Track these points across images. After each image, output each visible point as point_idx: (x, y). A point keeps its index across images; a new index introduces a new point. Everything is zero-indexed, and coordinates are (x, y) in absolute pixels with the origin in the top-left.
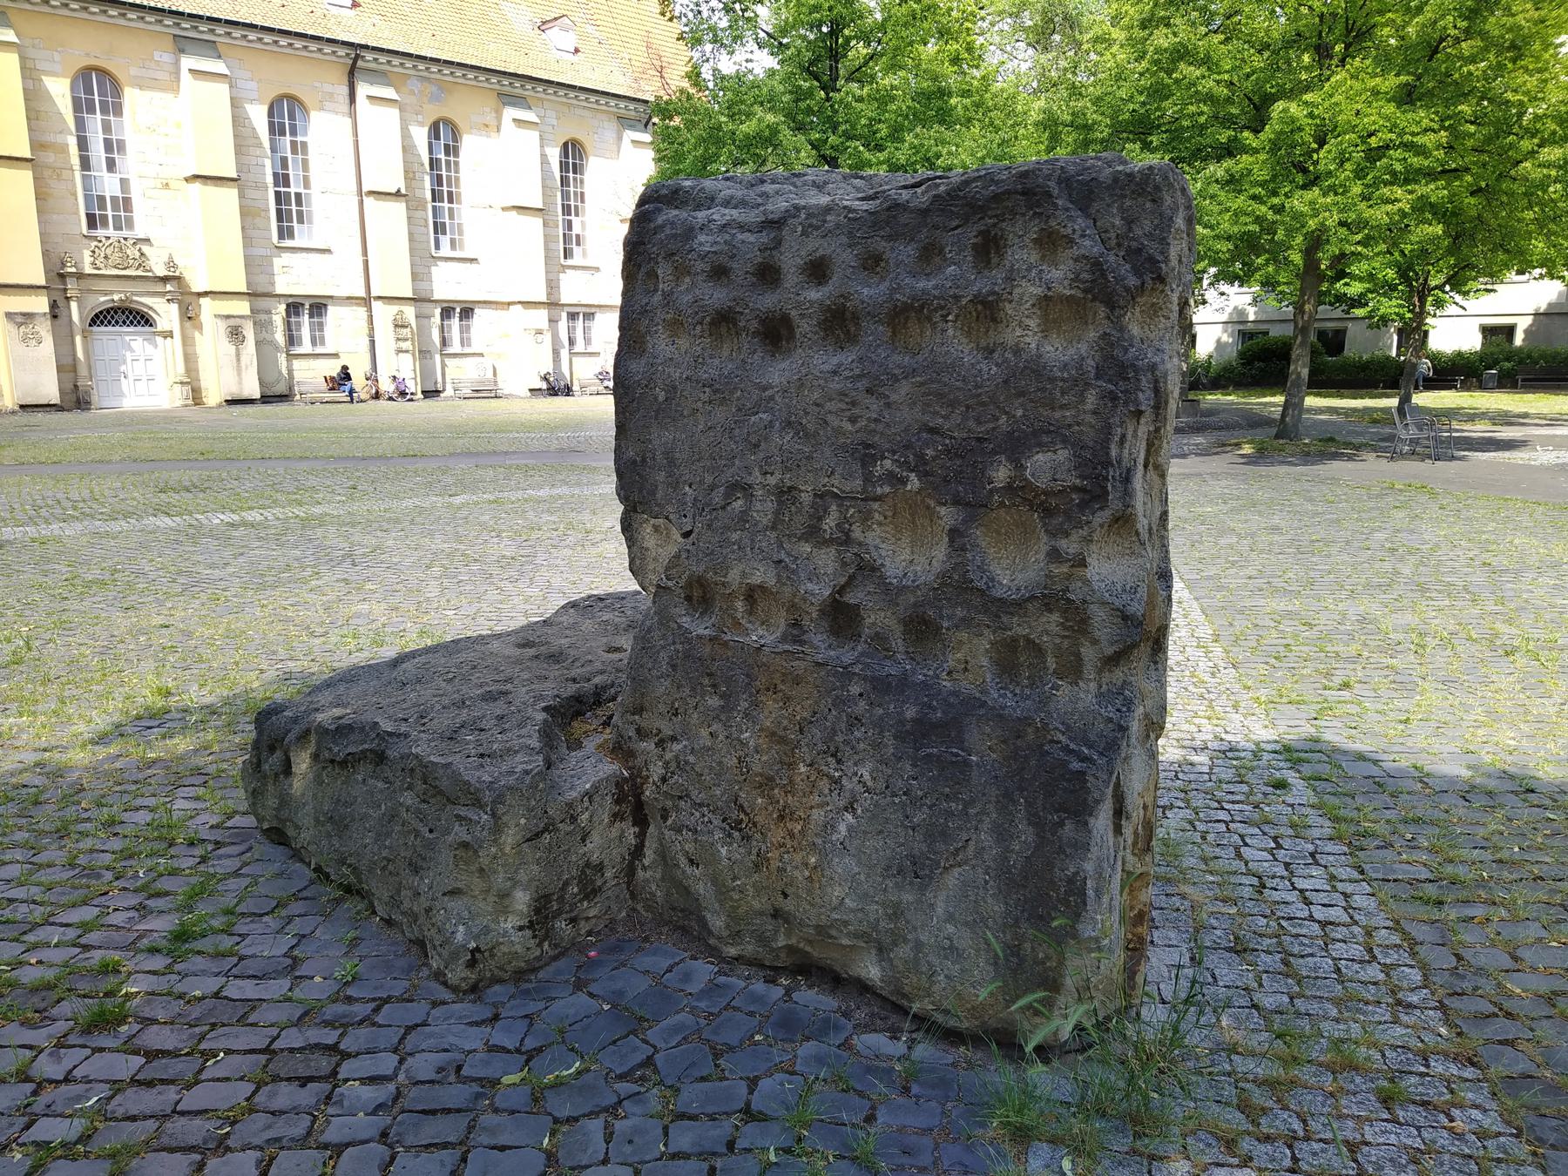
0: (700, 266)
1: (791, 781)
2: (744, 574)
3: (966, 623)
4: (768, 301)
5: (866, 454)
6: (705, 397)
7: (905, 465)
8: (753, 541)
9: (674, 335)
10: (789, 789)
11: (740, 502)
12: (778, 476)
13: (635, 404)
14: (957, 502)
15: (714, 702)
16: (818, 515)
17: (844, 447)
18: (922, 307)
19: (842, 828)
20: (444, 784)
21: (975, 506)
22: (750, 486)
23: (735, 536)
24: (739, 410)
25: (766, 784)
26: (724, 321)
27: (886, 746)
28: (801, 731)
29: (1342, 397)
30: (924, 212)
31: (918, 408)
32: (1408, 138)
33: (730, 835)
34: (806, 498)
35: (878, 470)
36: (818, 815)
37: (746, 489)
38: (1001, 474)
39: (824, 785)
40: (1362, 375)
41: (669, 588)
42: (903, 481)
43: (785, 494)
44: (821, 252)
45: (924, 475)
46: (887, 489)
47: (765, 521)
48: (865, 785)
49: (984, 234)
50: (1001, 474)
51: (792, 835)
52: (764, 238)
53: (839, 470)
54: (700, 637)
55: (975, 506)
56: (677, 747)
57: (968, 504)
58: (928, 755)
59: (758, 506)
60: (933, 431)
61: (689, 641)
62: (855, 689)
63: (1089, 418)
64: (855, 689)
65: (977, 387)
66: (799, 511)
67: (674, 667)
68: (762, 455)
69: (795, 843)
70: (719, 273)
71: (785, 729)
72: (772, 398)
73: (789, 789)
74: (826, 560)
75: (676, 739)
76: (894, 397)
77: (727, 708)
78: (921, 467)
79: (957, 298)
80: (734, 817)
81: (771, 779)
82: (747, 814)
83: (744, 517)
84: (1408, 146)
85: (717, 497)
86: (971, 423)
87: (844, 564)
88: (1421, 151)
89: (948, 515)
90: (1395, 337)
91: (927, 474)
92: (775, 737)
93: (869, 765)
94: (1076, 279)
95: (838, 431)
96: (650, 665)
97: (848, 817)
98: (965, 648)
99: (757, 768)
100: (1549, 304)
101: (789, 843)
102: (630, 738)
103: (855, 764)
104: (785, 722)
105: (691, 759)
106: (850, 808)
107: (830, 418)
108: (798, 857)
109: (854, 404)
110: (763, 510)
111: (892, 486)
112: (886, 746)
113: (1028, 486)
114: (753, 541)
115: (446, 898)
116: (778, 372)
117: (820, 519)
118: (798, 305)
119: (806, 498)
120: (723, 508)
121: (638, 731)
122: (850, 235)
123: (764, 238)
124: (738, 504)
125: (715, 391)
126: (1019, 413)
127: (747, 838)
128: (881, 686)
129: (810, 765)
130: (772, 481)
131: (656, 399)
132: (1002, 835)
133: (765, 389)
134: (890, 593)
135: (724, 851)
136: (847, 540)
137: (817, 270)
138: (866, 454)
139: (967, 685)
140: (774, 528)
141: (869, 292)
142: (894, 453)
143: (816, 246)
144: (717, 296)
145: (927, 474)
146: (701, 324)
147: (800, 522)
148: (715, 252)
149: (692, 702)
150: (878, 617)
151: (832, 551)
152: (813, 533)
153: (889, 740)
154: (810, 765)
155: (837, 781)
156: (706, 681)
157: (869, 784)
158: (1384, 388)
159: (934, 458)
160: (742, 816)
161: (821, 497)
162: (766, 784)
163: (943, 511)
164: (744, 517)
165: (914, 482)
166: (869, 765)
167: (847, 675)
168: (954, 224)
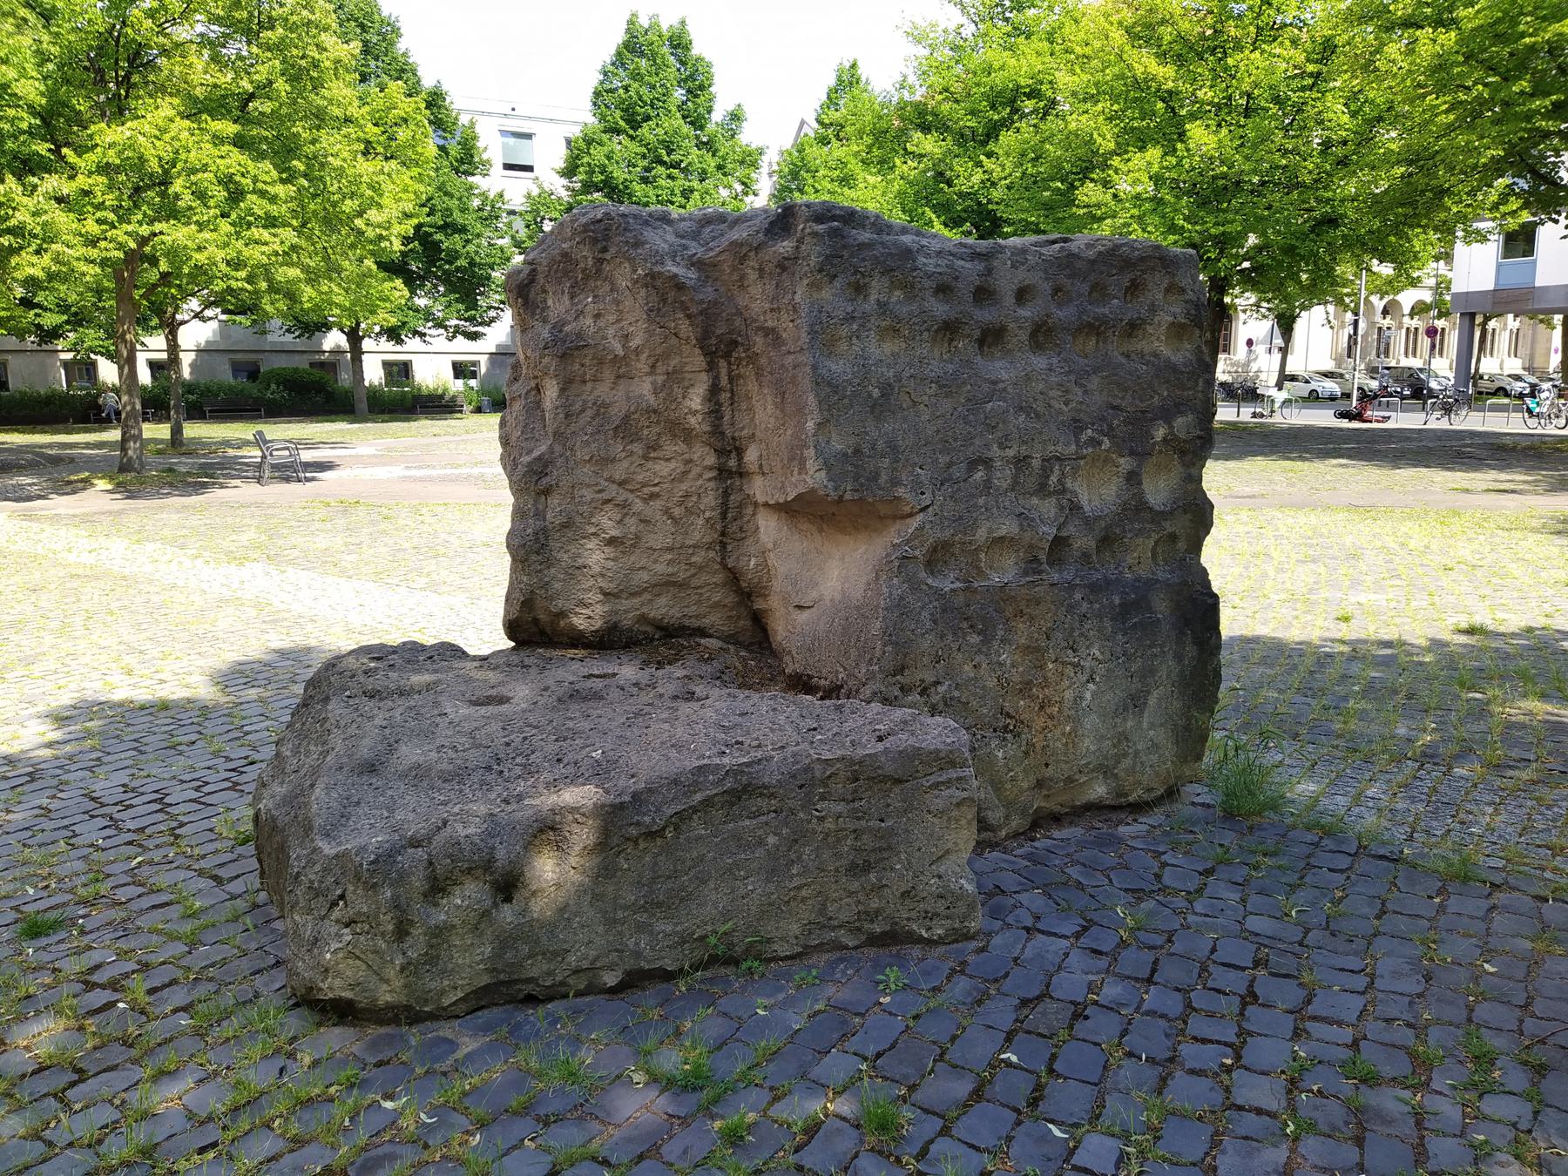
0: (927, 283)
1: (1045, 679)
2: (990, 530)
3: (1138, 534)
4: (985, 315)
5: (1077, 426)
6: (932, 392)
7: (1102, 433)
8: (997, 502)
9: (882, 339)
10: (1046, 683)
11: (980, 474)
12: (1015, 447)
13: (846, 401)
14: (1132, 453)
15: (974, 639)
16: (1045, 473)
17: (1063, 422)
18: (1100, 326)
19: (1088, 695)
20: (889, 769)
21: (1141, 454)
22: (991, 460)
23: (981, 501)
24: (969, 400)
25: (1025, 689)
26: (949, 329)
27: (1106, 628)
28: (1048, 638)
29: (69, 433)
30: (1093, 262)
31: (1105, 393)
32: (260, 185)
33: (1004, 739)
34: (1036, 463)
35: (1084, 437)
36: (1069, 695)
37: (987, 463)
38: (1160, 433)
39: (1069, 671)
40: (46, 410)
41: (915, 557)
42: (1100, 443)
43: (1021, 462)
44: (1027, 282)
45: (1112, 437)
46: (1090, 450)
47: (1005, 485)
48: (1097, 659)
49: (1133, 281)
50: (1160, 433)
51: (1051, 717)
52: (980, 266)
53: (1062, 440)
54: (953, 590)
55: (1141, 454)
56: (941, 689)
57: (1138, 454)
58: (1135, 624)
59: (999, 475)
60: (1115, 408)
61: (943, 596)
62: (1078, 596)
63: (1200, 395)
64: (1078, 596)
65: (1139, 378)
66: (1030, 474)
67: (935, 622)
68: (1000, 434)
69: (1055, 722)
70: (943, 290)
71: (1037, 640)
72: (1005, 389)
73: (1046, 683)
74: (1048, 507)
75: (939, 683)
76: (1090, 386)
77: (987, 641)
78: (1110, 433)
79: (1121, 320)
80: (1001, 724)
81: (1029, 683)
82: (1011, 717)
83: (988, 484)
84: (262, 194)
85: (958, 472)
86: (1137, 402)
87: (1062, 508)
88: (273, 199)
89: (1125, 463)
90: (63, 372)
91: (1114, 437)
92: (1028, 650)
93: (1096, 646)
94: (1188, 313)
95: (1060, 412)
96: (913, 627)
97: (1091, 686)
98: (1140, 548)
99: (1017, 679)
100: (207, 342)
101: (1050, 723)
102: (896, 697)
103: (1087, 648)
104: (1036, 635)
105: (956, 694)
106: (1091, 679)
107: (1053, 403)
108: (1058, 732)
109: (1067, 391)
110: (1003, 477)
111: (1094, 447)
112: (1106, 628)
113: (1176, 438)
114: (997, 502)
115: (934, 867)
116: (1000, 369)
117: (1048, 477)
118: (1016, 320)
119: (1036, 463)
120: (965, 480)
121: (902, 689)
122: (1046, 272)
123: (980, 266)
124: (979, 475)
125: (941, 387)
126: (1165, 394)
127: (1017, 735)
128: (1095, 588)
129: (1056, 661)
130: (1010, 453)
131: (870, 396)
132: (1179, 657)
133: (995, 383)
134: (1088, 522)
135: (1000, 754)
136: (1064, 491)
137: (1022, 295)
138: (1077, 426)
139: (1143, 572)
140: (1013, 490)
141: (1063, 314)
142: (1093, 424)
143: (1022, 276)
144: (940, 309)
145: (1114, 437)
146: (928, 330)
147: (1031, 482)
148: (940, 274)
149: (955, 646)
150: (1083, 541)
151: (1053, 500)
152: (1042, 490)
153: (1108, 624)
154: (1056, 661)
155: (1076, 665)
156: (965, 625)
157: (1100, 657)
158: (74, 423)
159: (1118, 426)
160: (1008, 721)
161: (1048, 461)
162: (1025, 689)
163: (1122, 461)
164: (988, 484)
165: (1106, 443)
166: (1096, 646)
167: (1072, 587)
168: (1114, 272)
